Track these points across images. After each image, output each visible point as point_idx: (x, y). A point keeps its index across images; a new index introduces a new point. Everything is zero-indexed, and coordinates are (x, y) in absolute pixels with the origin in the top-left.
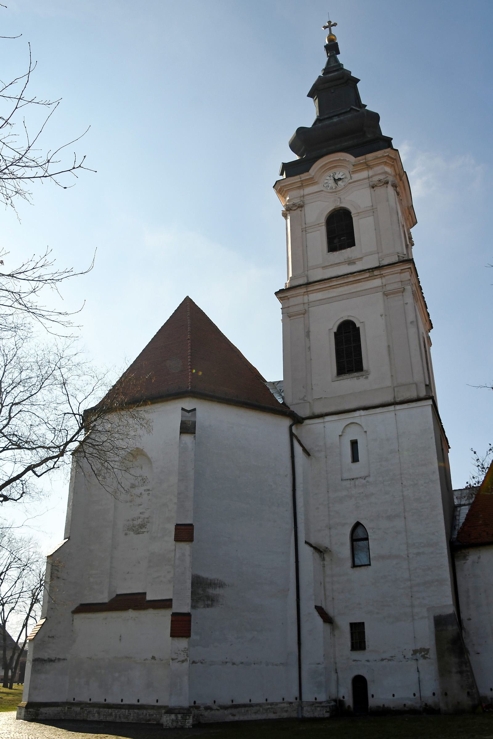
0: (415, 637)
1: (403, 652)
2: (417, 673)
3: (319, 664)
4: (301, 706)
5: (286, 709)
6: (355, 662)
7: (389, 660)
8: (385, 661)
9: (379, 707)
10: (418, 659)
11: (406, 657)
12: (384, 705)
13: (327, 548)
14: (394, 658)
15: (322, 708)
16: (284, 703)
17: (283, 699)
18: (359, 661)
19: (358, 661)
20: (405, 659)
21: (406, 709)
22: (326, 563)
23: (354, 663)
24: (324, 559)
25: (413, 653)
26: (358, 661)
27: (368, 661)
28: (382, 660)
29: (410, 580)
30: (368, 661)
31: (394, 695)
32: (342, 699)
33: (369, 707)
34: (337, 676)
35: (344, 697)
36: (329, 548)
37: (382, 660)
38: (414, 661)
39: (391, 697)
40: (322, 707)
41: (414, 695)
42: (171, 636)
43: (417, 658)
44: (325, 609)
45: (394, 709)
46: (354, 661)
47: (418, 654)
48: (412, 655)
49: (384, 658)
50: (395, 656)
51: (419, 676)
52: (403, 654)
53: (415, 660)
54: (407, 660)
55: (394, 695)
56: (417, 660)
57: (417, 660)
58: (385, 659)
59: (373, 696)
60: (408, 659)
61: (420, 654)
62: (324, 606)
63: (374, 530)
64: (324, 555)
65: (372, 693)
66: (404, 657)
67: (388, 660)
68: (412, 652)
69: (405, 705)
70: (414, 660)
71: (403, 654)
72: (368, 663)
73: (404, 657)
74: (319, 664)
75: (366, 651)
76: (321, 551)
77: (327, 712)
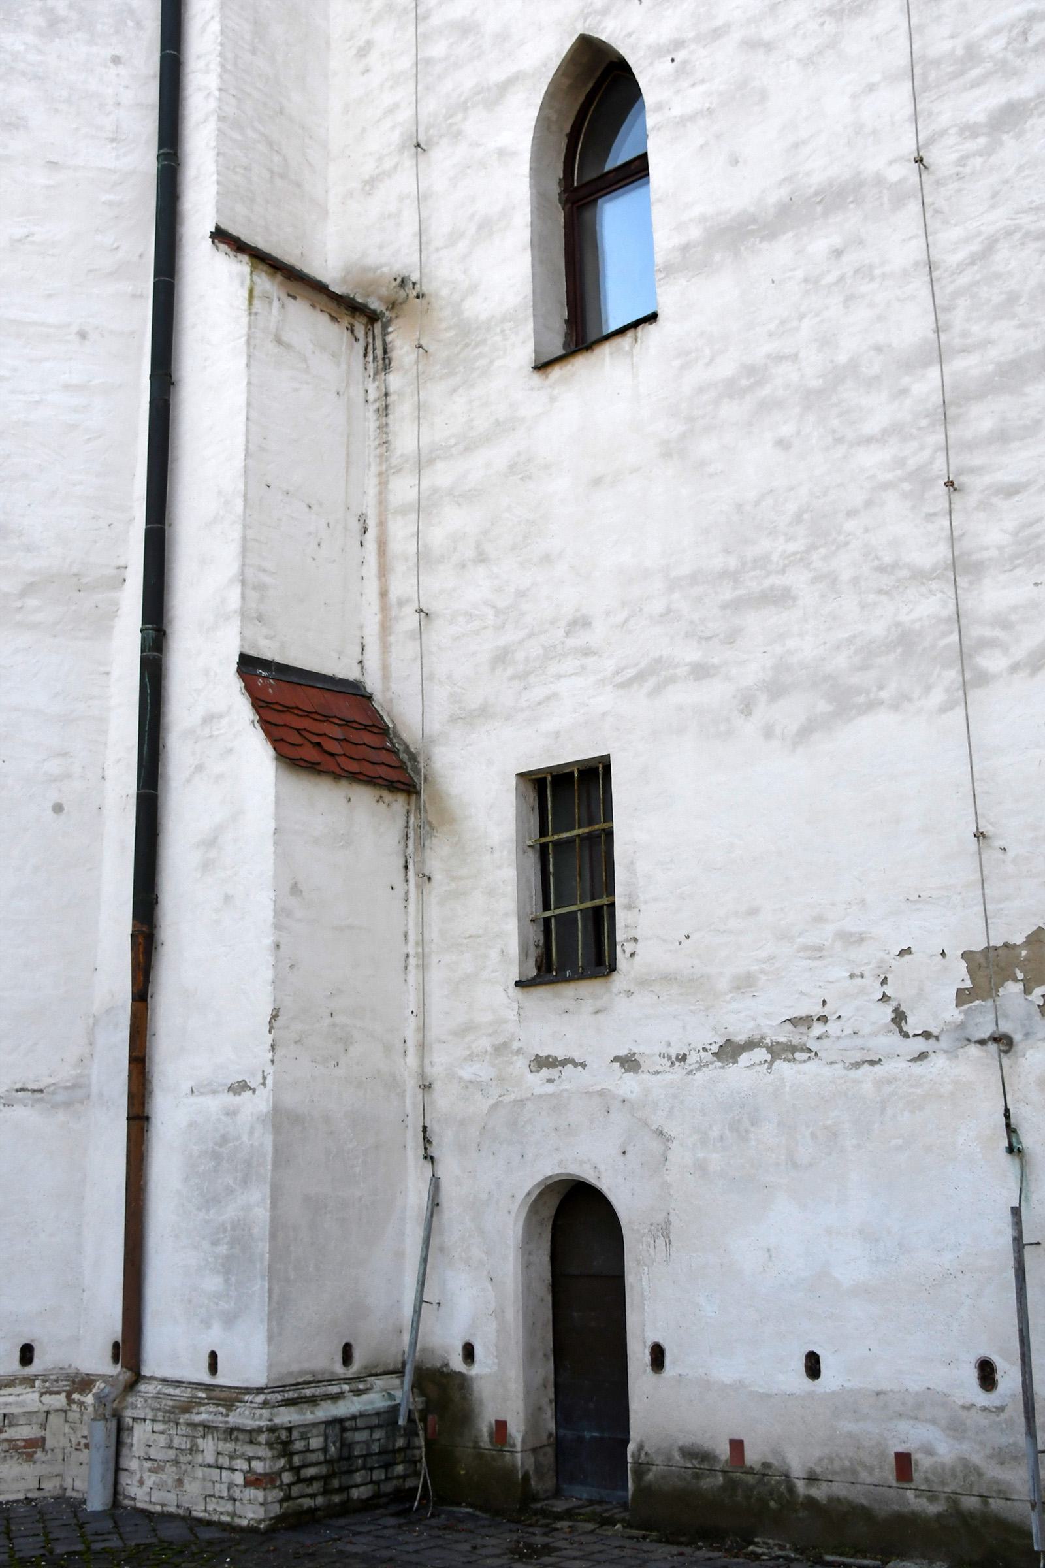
0: (980, 835)
1: (884, 981)
2: (1009, 1164)
3: (240, 1087)
4: (118, 1417)
5: (24, 1432)
6: (545, 1072)
7: (780, 1051)
8: (745, 1058)
9: (699, 1456)
10: (1017, 1037)
11: (913, 1024)
12: (737, 1446)
13: (403, 283)
14: (818, 1029)
15: (229, 1447)
16: (29, 1381)
17: (27, 1354)
18: (570, 1066)
19: (564, 1062)
20: (906, 1035)
21: (913, 1501)
22: (395, 380)
23: (536, 1082)
24: (386, 363)
25: (968, 984)
26: (564, 1062)
27: (629, 1063)
28: (729, 1051)
29: (940, 355)
30: (629, 1063)
31: (813, 1365)
32: (457, 1363)
33: (631, 1447)
34: (435, 1183)
35: (469, 1352)
36: (415, 277)
37: (729, 1051)
38: (974, 1050)
39: (795, 1378)
40: (231, 1433)
41: (987, 1374)
42: (537, 1055)
43: (1005, 1027)
44: (378, 697)
45: (819, 1493)
46: (542, 1062)
47: (1013, 989)
48: (963, 997)
49: (741, 1038)
50: (823, 1019)
51: (433, 1172)
52: (885, 998)
53: (993, 1047)
54: (920, 1045)
55: (813, 1365)
56: (1004, 1042)
57: (1004, 1042)
58: (750, 1045)
59: (658, 1356)
60: (927, 1035)
61: (1027, 991)
62: (373, 684)
63: (680, 56)
64: (385, 334)
65: (652, 1337)
66: (899, 1017)
67: (770, 1049)
68: (960, 975)
69: (904, 1462)
70: (982, 1042)
71: (885, 998)
72: (629, 1085)
73: (899, 1017)
74: (240, 1087)
75: (619, 981)
76: (374, 312)
77: (252, 1481)
